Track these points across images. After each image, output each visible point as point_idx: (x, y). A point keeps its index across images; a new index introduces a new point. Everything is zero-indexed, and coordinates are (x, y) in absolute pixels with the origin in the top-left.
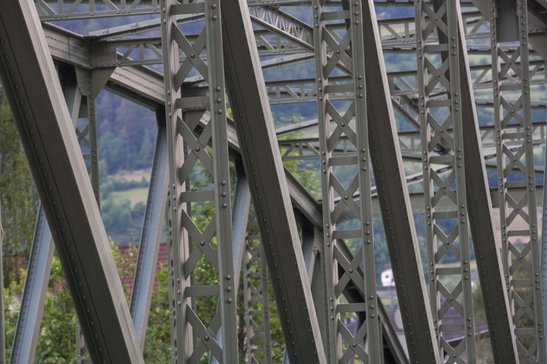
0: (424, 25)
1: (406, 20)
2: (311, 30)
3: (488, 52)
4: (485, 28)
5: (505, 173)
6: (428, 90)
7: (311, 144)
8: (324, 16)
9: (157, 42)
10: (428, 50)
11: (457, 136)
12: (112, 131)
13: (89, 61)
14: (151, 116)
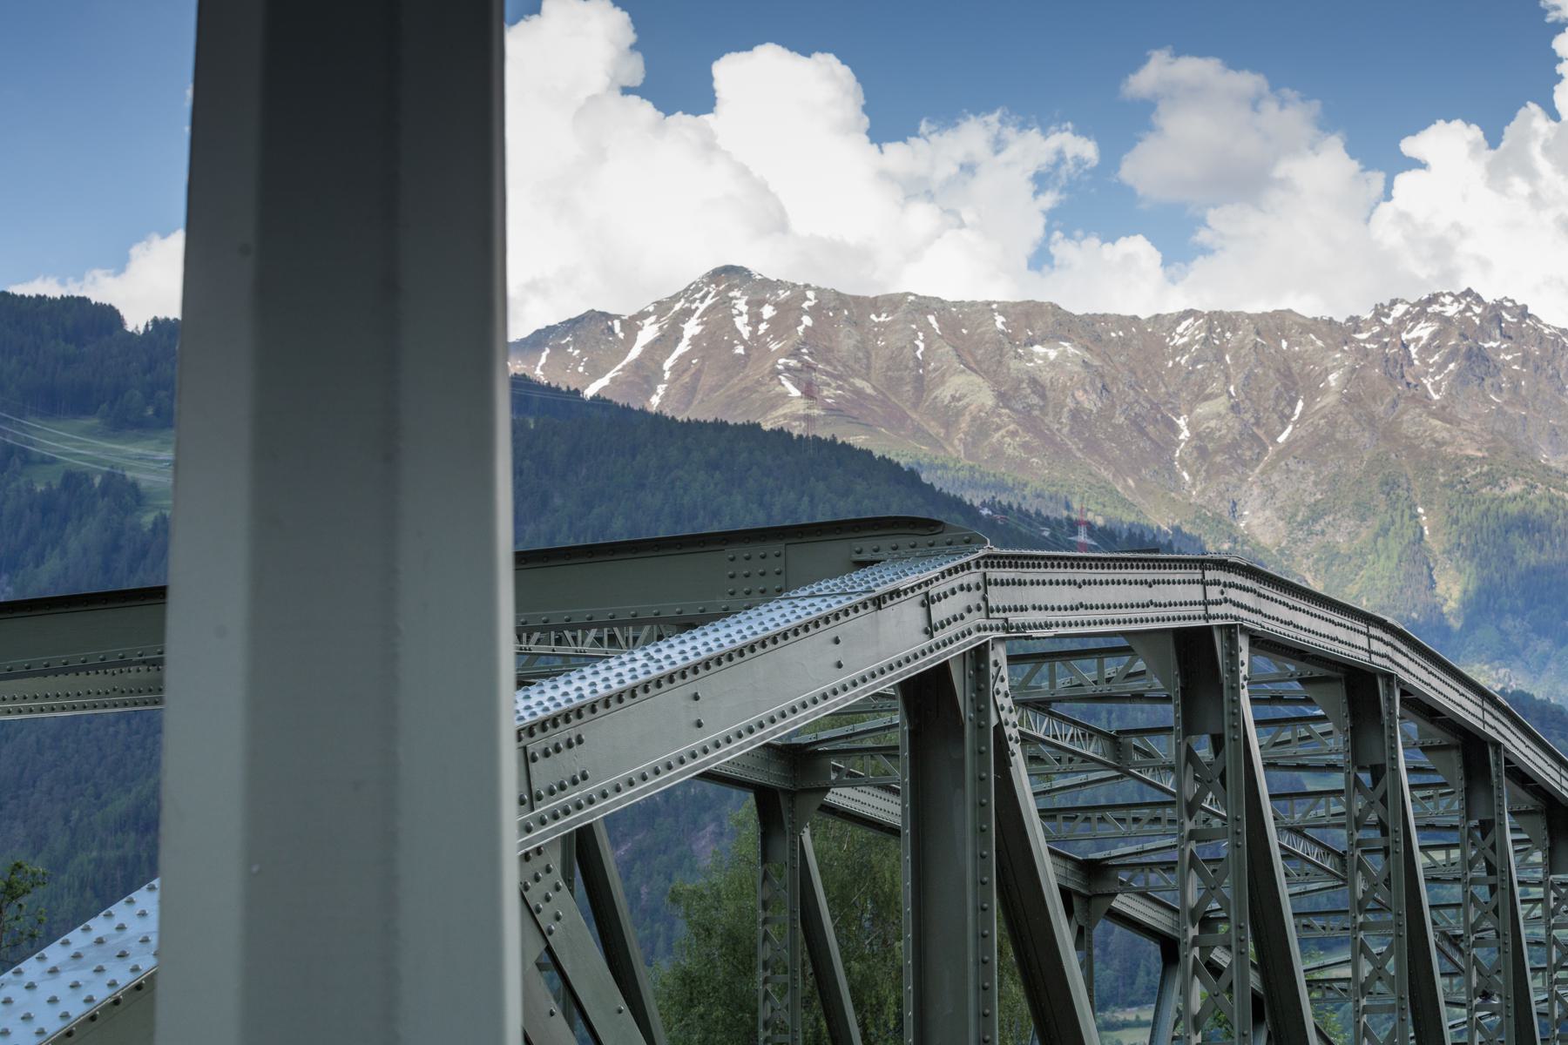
1: (1447, 847)
3: (1540, 884)
4: (1537, 857)
5: (1558, 1023)
6: (1474, 928)
7: (1336, 985)
9: (1169, 867)
10: (1473, 881)
11: (1506, 980)
12: (1103, 961)
13: (1087, 887)
14: (1154, 949)
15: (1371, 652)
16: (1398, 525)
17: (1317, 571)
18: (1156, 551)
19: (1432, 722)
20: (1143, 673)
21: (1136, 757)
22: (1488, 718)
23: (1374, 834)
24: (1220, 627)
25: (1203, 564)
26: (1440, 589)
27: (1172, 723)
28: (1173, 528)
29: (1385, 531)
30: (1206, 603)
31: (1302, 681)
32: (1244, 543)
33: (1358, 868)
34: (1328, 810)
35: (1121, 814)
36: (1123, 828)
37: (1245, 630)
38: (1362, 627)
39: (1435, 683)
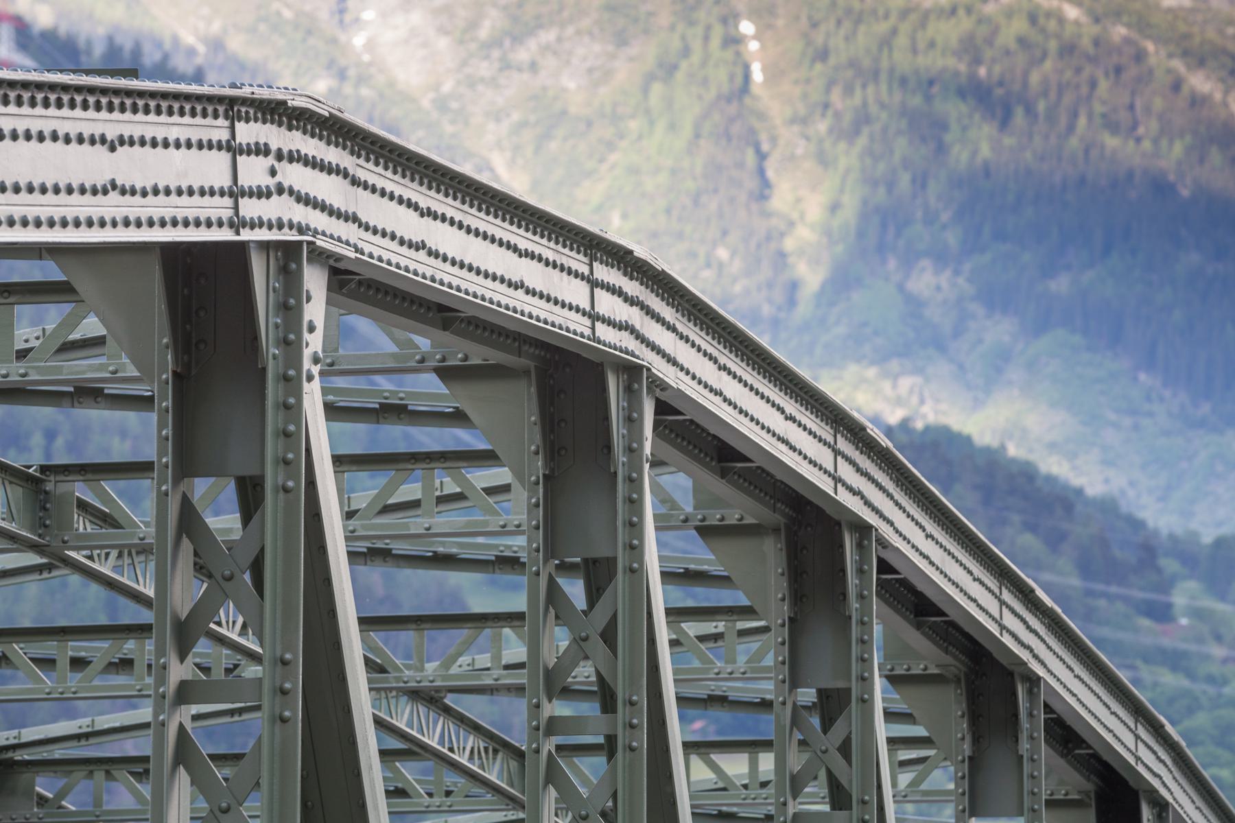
0: (796, 761)
1: (754, 746)
2: (519, 755)
4: (943, 778)
8: (553, 727)
9: (139, 767)
15: (594, 317)
16: (696, 58)
17: (517, 149)
18: (133, 73)
19: (723, 474)
20: (99, 342)
21: (82, 525)
22: (846, 472)
23: (589, 709)
24: (265, 246)
25: (232, 107)
26: (781, 199)
27: (149, 452)
28: (206, 41)
29: (667, 69)
30: (236, 193)
31: (446, 373)
32: (361, 80)
33: (549, 780)
34: (497, 657)
35: (47, 648)
36: (47, 681)
37: (319, 256)
38: (578, 262)
39: (733, 389)
